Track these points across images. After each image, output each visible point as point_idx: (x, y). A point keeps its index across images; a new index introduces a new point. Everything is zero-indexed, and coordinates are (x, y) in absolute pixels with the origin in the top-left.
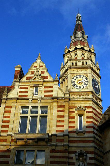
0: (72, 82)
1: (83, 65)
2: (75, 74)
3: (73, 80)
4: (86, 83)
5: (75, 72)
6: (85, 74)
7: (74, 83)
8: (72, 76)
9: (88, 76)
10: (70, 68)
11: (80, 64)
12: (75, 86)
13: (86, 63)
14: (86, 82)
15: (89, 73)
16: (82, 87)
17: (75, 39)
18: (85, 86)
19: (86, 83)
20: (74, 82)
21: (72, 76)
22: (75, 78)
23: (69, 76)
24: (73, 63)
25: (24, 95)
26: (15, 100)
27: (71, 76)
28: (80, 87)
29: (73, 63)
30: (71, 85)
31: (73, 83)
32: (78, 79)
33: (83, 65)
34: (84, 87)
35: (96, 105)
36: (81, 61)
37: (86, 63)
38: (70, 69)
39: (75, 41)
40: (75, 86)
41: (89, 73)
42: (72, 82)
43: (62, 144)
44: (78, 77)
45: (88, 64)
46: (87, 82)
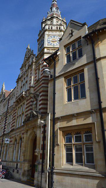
5: (51, 33)
8: (48, 36)
13: (51, 28)
16: (55, 45)
21: (48, 36)
24: (57, 28)
36: (56, 26)
40: (50, 44)
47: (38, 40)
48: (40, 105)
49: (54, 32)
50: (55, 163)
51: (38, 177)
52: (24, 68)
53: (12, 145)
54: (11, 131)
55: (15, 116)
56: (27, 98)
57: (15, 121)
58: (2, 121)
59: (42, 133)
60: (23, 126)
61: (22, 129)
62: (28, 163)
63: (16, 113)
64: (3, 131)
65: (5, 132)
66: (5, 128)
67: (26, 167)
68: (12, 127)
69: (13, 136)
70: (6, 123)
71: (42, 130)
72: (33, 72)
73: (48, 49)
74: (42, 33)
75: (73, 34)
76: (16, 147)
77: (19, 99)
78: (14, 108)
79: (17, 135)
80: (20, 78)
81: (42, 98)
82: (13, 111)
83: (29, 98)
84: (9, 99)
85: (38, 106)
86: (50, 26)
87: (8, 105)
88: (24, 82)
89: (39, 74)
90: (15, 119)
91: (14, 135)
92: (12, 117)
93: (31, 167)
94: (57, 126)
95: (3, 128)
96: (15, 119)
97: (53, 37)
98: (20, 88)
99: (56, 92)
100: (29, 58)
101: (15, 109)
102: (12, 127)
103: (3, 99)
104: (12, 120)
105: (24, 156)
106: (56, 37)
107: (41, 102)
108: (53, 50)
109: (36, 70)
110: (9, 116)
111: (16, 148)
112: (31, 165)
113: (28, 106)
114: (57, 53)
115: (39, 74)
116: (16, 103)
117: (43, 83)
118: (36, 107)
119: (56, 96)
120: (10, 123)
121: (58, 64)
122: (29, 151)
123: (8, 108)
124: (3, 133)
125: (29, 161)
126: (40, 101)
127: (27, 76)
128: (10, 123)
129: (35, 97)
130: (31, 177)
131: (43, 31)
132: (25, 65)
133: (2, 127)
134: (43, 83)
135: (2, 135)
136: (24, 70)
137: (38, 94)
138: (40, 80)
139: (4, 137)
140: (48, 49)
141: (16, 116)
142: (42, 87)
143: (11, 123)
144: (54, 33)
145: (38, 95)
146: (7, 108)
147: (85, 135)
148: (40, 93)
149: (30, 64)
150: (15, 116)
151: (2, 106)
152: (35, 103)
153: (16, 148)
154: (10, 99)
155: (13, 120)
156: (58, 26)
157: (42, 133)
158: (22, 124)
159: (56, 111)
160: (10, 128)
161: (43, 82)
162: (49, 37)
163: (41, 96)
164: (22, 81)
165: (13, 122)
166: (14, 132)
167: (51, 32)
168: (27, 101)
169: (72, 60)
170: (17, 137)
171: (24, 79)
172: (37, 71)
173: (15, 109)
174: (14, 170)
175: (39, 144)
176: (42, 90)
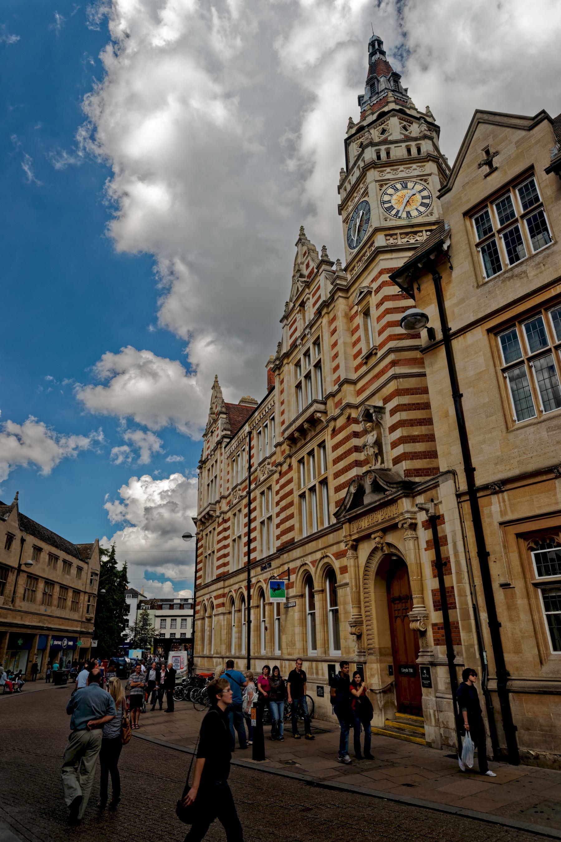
0: (384, 202)
1: (379, 157)
2: (389, 180)
3: (386, 198)
4: (427, 201)
5: (388, 173)
6: (418, 176)
7: (389, 205)
8: (381, 186)
9: (430, 181)
10: (373, 165)
11: (398, 152)
12: (394, 212)
13: (388, 154)
14: (423, 198)
15: (430, 175)
16: (414, 213)
17: (374, 98)
18: (422, 209)
19: (427, 201)
20: (389, 202)
21: (381, 186)
22: (390, 191)
23: (373, 188)
24: (409, 151)
25: (382, 378)
26: (517, 830)
27: (378, 186)
28: (408, 213)
29: (409, 151)
30: (381, 210)
31: (386, 205)
32: (399, 193)
33: (379, 157)
34: (420, 213)
35: (478, 269)
36: (404, 145)
37: (388, 154)
38: (373, 170)
39: (375, 102)
40: (394, 212)
41: (430, 175)
42: (384, 202)
43: (528, 566)
44: (399, 186)
45: (424, 149)
46: (428, 197)
47: (341, 208)
48: (394, 445)
49: (401, 168)
50: (508, 657)
51: (439, 710)
52: (299, 316)
53: (296, 600)
54: (283, 550)
55: (291, 492)
56: (332, 424)
57: (293, 510)
58: (232, 516)
59: (426, 550)
60: (333, 529)
61: (331, 538)
62: (381, 662)
63: (290, 481)
64: (246, 549)
65: (252, 556)
66: (250, 541)
67: (372, 675)
68: (284, 533)
69: (292, 565)
70: (250, 521)
71: (425, 535)
72: (340, 323)
73: (392, 232)
74: (353, 179)
75: (496, 162)
76: (266, 613)
77: (301, 429)
78: (281, 464)
79: (313, 563)
80: (287, 355)
81: (398, 417)
82: (276, 476)
83: (341, 422)
84: (250, 433)
85: (386, 448)
86: (383, 148)
87: (250, 457)
88: (307, 366)
89: (366, 329)
90: (291, 504)
91: (298, 563)
92: (273, 498)
93: (391, 674)
94: (490, 515)
95: (245, 539)
96: (291, 504)
97: (399, 186)
98: (293, 390)
99: (462, 389)
100: (313, 276)
101: (285, 467)
102: (284, 533)
103: (224, 437)
104: (277, 509)
105: (359, 637)
106: (410, 185)
107: (398, 434)
108: (407, 234)
109: (352, 319)
110: (262, 493)
111: (264, 617)
112: (390, 667)
113: (341, 451)
114: (444, 243)
115: (366, 329)
116: (285, 447)
117: (394, 363)
118: (380, 453)
119: (467, 404)
120: (270, 518)
121: (452, 285)
122: (374, 616)
123: (250, 467)
124: (246, 559)
125: (382, 653)
126: (393, 429)
127: (317, 343)
128: (270, 518)
129: (368, 417)
130: (399, 711)
131: (357, 173)
132: (303, 305)
133: (240, 537)
134: (394, 363)
135: (241, 565)
136: (300, 325)
137: (380, 404)
138: (380, 354)
139: (253, 573)
140: (391, 235)
141: (296, 494)
142: (395, 377)
143: (276, 521)
144: (402, 172)
145: (380, 410)
146: (247, 466)
147: (535, 554)
148: (386, 400)
149: (323, 298)
150: (291, 492)
151: (225, 462)
152: (371, 438)
153: (264, 617)
154: (255, 433)
155: (283, 509)
156: (413, 144)
157: (426, 550)
158: (334, 521)
159: (475, 461)
160: (272, 538)
161: (392, 357)
162: (385, 187)
163: (393, 412)
164: (298, 365)
165: (283, 516)
166: (297, 553)
167: (388, 169)
168: (335, 432)
169: (508, 261)
170: (312, 570)
171: (307, 354)
172: (359, 320)
173: (285, 467)
174: (322, 688)
175: (422, 591)
176: (392, 387)
